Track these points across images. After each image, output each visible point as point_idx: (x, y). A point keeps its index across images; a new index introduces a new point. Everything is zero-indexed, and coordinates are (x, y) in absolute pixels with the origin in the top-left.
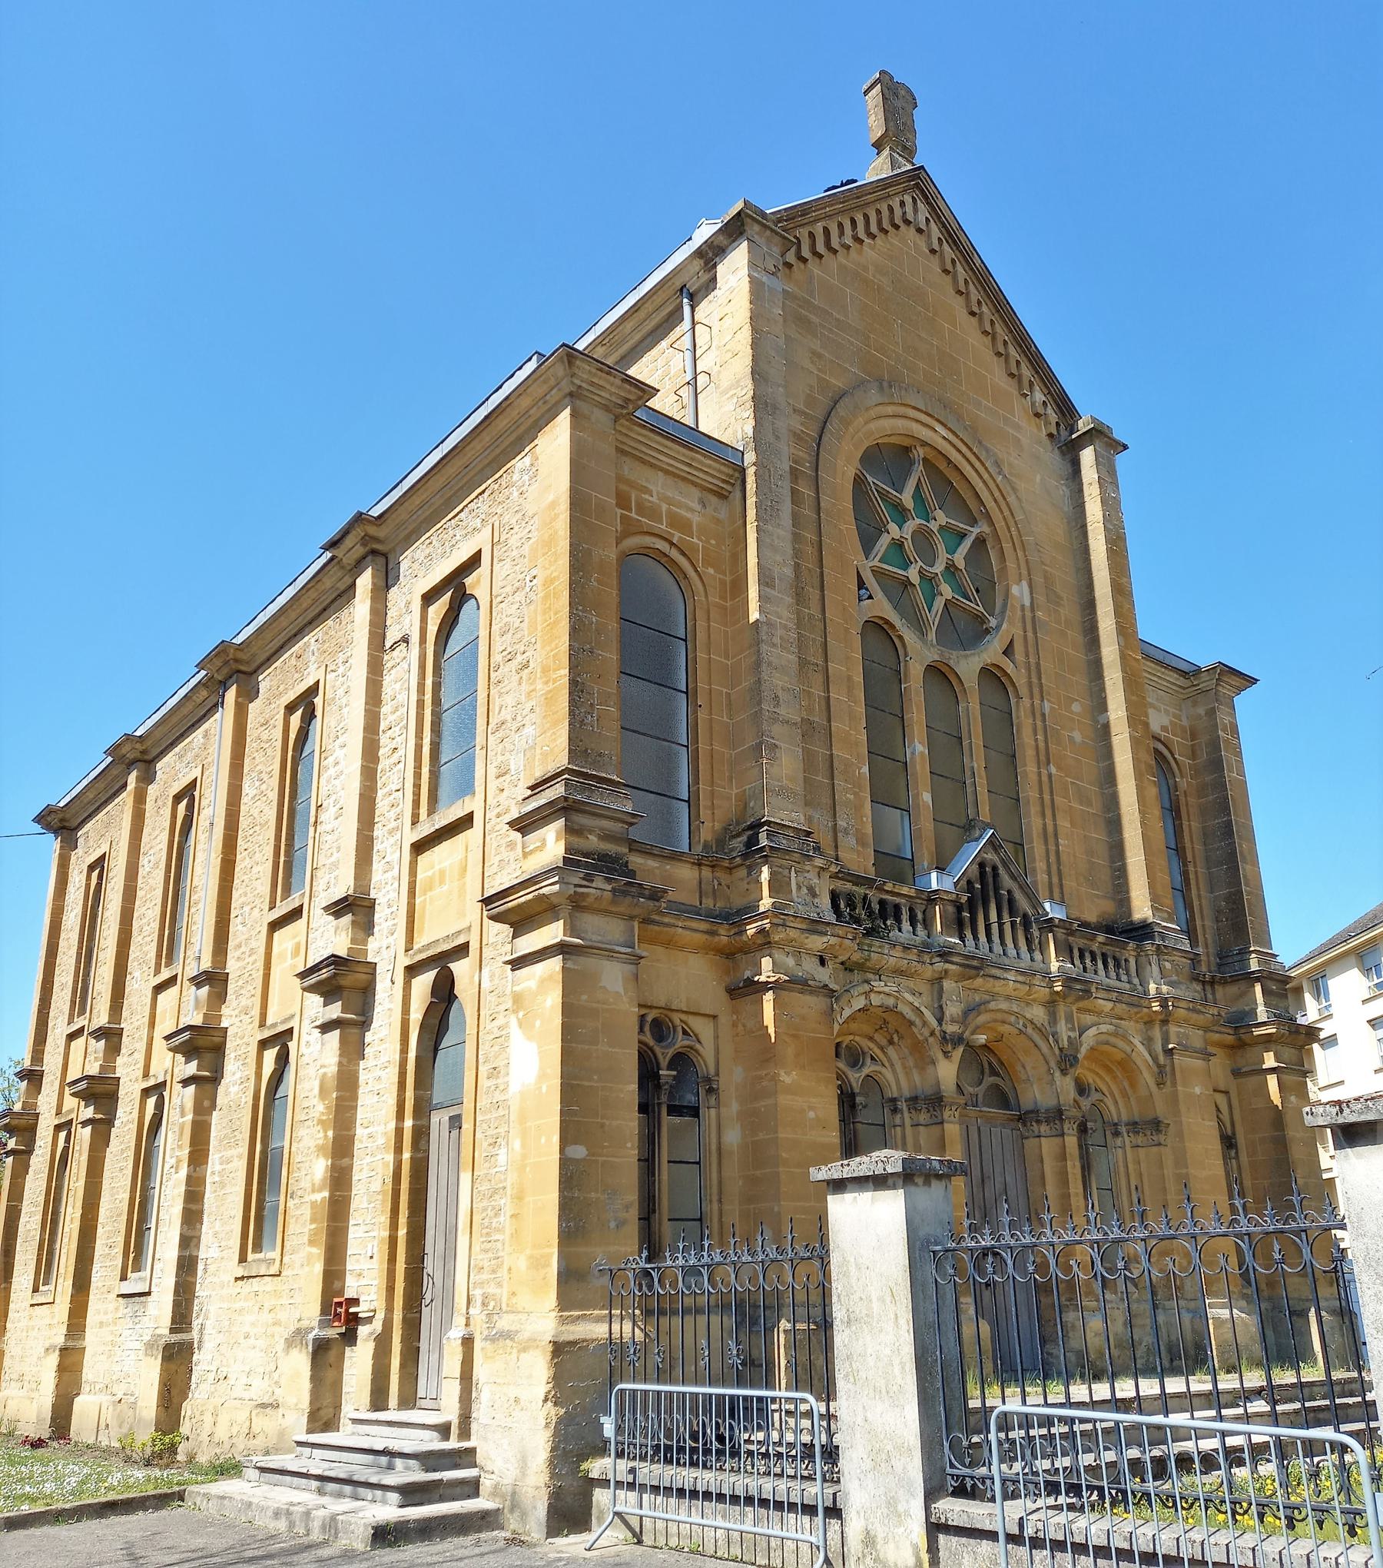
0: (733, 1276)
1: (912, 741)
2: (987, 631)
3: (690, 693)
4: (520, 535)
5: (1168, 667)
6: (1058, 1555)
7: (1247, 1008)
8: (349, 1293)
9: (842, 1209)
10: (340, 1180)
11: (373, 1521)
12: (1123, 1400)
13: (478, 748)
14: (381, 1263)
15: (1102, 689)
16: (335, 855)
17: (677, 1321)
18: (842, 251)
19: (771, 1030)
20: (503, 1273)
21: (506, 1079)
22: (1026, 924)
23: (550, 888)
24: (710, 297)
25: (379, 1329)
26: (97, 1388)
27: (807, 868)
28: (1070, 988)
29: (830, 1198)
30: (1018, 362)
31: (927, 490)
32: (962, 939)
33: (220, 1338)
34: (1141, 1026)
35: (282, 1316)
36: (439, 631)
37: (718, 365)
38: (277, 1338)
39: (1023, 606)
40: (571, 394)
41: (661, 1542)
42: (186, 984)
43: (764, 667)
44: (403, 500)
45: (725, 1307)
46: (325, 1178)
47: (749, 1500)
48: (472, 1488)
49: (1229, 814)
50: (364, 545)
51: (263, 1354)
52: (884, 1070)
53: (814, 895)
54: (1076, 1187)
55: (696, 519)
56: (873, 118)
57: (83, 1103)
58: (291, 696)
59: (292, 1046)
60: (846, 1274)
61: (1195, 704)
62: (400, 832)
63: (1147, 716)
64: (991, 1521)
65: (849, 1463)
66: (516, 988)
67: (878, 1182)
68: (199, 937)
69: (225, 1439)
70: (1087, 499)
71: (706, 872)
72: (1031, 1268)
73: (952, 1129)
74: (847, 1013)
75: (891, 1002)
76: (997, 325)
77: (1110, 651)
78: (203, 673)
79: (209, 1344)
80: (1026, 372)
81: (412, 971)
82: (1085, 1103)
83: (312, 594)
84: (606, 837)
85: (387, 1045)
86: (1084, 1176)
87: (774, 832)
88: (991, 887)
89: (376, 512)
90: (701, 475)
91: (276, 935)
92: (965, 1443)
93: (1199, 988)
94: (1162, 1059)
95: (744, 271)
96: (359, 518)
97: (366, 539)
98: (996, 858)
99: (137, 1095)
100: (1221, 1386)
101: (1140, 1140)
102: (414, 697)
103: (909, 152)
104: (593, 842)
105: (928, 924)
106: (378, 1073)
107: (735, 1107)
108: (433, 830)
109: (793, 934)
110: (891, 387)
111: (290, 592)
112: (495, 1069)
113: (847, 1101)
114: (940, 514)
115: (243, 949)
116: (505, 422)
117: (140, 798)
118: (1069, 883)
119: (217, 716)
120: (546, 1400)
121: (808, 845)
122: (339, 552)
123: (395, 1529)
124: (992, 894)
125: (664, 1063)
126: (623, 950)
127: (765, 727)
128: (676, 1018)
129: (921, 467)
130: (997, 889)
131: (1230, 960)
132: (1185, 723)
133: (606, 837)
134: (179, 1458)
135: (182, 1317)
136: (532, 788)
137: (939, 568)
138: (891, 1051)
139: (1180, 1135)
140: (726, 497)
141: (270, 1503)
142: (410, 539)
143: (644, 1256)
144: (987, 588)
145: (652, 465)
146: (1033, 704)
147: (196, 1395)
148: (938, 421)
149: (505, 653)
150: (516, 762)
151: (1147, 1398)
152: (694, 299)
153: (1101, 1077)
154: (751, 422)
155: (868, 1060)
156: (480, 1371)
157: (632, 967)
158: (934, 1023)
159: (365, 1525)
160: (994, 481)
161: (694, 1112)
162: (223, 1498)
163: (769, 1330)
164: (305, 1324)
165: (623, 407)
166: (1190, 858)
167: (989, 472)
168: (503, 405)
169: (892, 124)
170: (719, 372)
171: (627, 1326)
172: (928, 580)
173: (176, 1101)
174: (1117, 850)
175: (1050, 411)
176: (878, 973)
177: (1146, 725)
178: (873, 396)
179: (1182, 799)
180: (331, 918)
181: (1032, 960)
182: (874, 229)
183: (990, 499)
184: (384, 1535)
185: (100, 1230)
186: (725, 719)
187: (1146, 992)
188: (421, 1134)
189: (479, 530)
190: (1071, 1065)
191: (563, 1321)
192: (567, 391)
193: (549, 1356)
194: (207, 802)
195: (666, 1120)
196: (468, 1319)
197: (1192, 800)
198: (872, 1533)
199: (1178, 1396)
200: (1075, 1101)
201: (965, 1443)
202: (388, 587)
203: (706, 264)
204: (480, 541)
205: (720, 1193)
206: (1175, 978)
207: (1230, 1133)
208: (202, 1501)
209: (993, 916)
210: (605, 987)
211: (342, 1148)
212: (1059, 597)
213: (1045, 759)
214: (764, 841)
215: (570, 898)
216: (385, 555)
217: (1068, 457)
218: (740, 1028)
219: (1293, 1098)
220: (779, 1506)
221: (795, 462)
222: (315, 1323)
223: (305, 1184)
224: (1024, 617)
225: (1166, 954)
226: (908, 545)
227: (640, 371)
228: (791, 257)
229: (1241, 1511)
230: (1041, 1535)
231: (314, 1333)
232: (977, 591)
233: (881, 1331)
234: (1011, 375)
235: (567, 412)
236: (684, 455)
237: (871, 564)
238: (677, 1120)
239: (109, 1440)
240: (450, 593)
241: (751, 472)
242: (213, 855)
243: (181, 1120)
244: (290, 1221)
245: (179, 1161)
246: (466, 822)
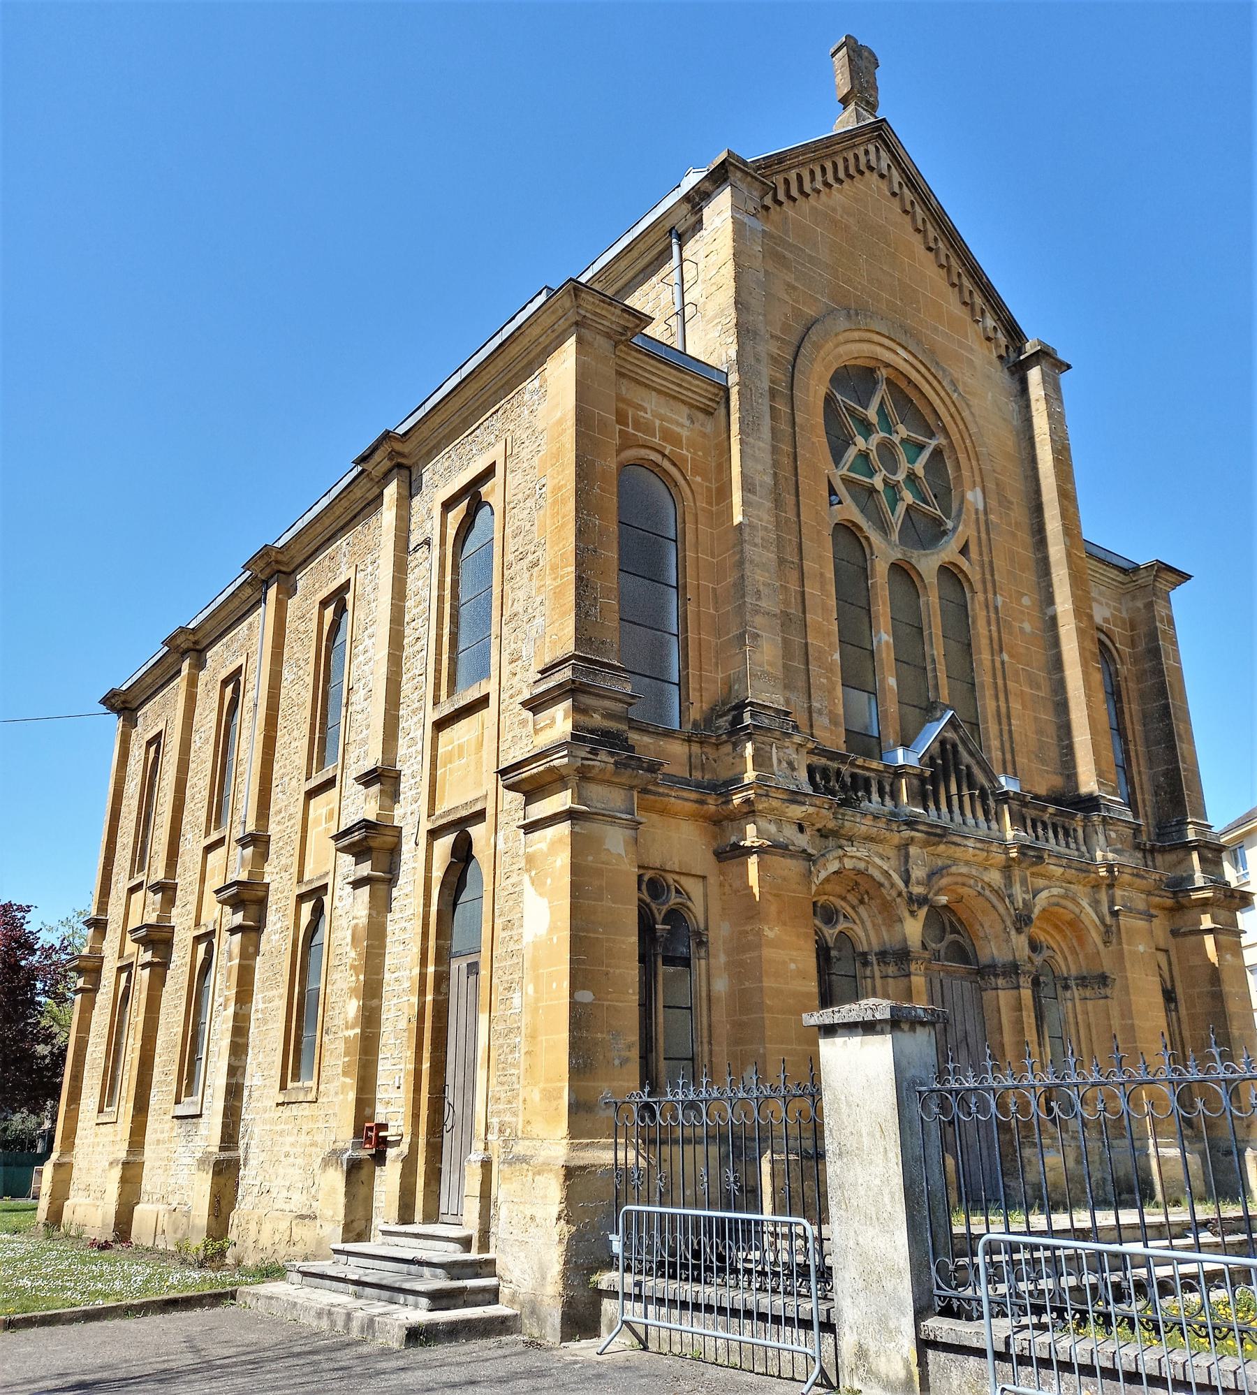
0: (730, 1111)
1: (878, 632)
2: (945, 533)
3: (680, 588)
4: (530, 449)
5: (1109, 564)
6: (1043, 1371)
7: (1184, 875)
8: (379, 1119)
9: (832, 1052)
10: (370, 1019)
11: (408, 1323)
12: (1082, 1230)
13: (493, 637)
14: (407, 1092)
15: (1050, 585)
16: (365, 732)
17: (677, 1150)
18: (813, 195)
19: (756, 890)
21: (520, 931)
22: (984, 796)
23: (559, 761)
24: (697, 237)
25: (406, 1151)
26: (155, 1198)
27: (786, 744)
28: (1024, 854)
29: (821, 1041)
30: (971, 292)
31: (889, 403)
32: (926, 810)
33: (263, 1156)
34: (1088, 889)
35: (319, 1138)
36: (457, 534)
37: (704, 297)
38: (314, 1157)
39: (977, 511)
40: (577, 323)
41: (665, 1349)
42: (233, 844)
44: (425, 419)
45: (723, 1139)
46: (356, 1018)
47: (748, 1314)
48: (492, 1295)
49: (1167, 698)
50: (391, 459)
51: (301, 1171)
52: (855, 927)
53: (793, 769)
54: (1031, 1035)
55: (685, 433)
56: (840, 77)
57: (142, 948)
59: (327, 900)
60: (838, 1111)
61: (1134, 598)
62: (422, 712)
63: (1091, 608)
64: (978, 1339)
65: (844, 1281)
67: (868, 1027)
68: (244, 804)
69: (269, 1246)
70: (1034, 413)
71: (696, 748)
72: (1013, 1109)
73: (918, 981)
74: (823, 875)
75: (862, 865)
76: (952, 259)
77: (1056, 550)
78: (248, 573)
79: (253, 1162)
80: (978, 300)
81: (434, 834)
82: (1038, 960)
83: (345, 503)
84: (609, 715)
85: (412, 900)
86: (1037, 1025)
87: (756, 712)
88: (951, 763)
89: (401, 430)
90: (690, 394)
91: (312, 802)
92: (951, 1267)
93: (1140, 855)
94: (1108, 919)
95: (728, 213)
96: (387, 436)
97: (393, 454)
98: (955, 736)
99: (190, 942)
100: (1171, 1219)
101: (1088, 993)
102: (435, 593)
103: (872, 107)
104: (597, 720)
105: (895, 795)
106: (404, 924)
107: (723, 959)
108: (452, 709)
109: (775, 803)
110: (857, 314)
111: (325, 502)
112: (509, 921)
113: (823, 954)
114: (901, 428)
115: (283, 815)
116: (517, 349)
117: (192, 683)
118: (1021, 760)
119: (260, 610)
120: (559, 1218)
121: (788, 724)
122: (369, 466)
123: (426, 1330)
125: (659, 918)
126: (624, 816)
127: (748, 617)
128: (670, 878)
129: (884, 387)
131: (1169, 830)
132: (1124, 615)
133: (609, 715)
134: (227, 1261)
135: (230, 1137)
136: (542, 672)
137: (901, 476)
138: (861, 909)
139: (1126, 989)
140: (712, 414)
141: (313, 1304)
142: (431, 454)
143: (646, 1090)
144: (944, 494)
145: (647, 386)
146: (986, 599)
147: (242, 1207)
148: (899, 344)
149: (517, 553)
150: (526, 650)
151: (1103, 1228)
152: (682, 239)
153: (1048, 933)
154: (735, 347)
155: (842, 918)
156: (500, 1191)
157: (632, 832)
158: (901, 884)
159: (400, 1327)
160: (951, 398)
161: (686, 962)
162: (271, 1298)
163: (755, 1162)
164: (340, 1145)
165: (622, 334)
167: (945, 390)
168: (516, 334)
169: (856, 82)
170: (705, 303)
171: (632, 1154)
172: (892, 487)
173: (224, 947)
174: (1065, 730)
175: (1000, 335)
176: (850, 840)
177: (1091, 617)
178: (842, 323)
179: (1123, 684)
180: (362, 787)
181: (989, 828)
182: (841, 175)
183: (947, 414)
184: (415, 1335)
185: (157, 1059)
186: (711, 611)
187: (1093, 859)
188: (442, 979)
189: (493, 445)
190: (1026, 925)
191: (574, 1148)
192: (573, 320)
193: (561, 1179)
194: (251, 685)
195: (661, 969)
196: (486, 1144)
197: (1131, 685)
198: (865, 1347)
199: (1132, 1227)
200: (1029, 958)
201: (951, 1267)
202: (411, 497)
203: (693, 208)
204: (495, 454)
205: (710, 1036)
206: (1119, 846)
207: (1169, 987)
208: (252, 1301)
209: (954, 789)
210: (608, 850)
211: (372, 991)
212: (1009, 502)
213: (998, 647)
214: (747, 720)
215: (578, 770)
216: (409, 468)
217: (1017, 376)
218: (727, 887)
219: (1228, 957)
220: (776, 1320)
222: (349, 1145)
223: (339, 1021)
224: (977, 519)
225: (1111, 824)
226: (874, 456)
227: (635, 301)
228: (768, 201)
229: (1220, 1336)
230: (1026, 1353)
231: (348, 1154)
232: (935, 497)
233: (871, 1163)
234: (965, 303)
235: (573, 339)
236: (674, 376)
237: (840, 473)
238: (671, 969)
239: (167, 1244)
240: (467, 501)
241: (734, 392)
242: (257, 732)
243: (229, 964)
244: (325, 1053)
245: (227, 1000)
246: (483, 702)
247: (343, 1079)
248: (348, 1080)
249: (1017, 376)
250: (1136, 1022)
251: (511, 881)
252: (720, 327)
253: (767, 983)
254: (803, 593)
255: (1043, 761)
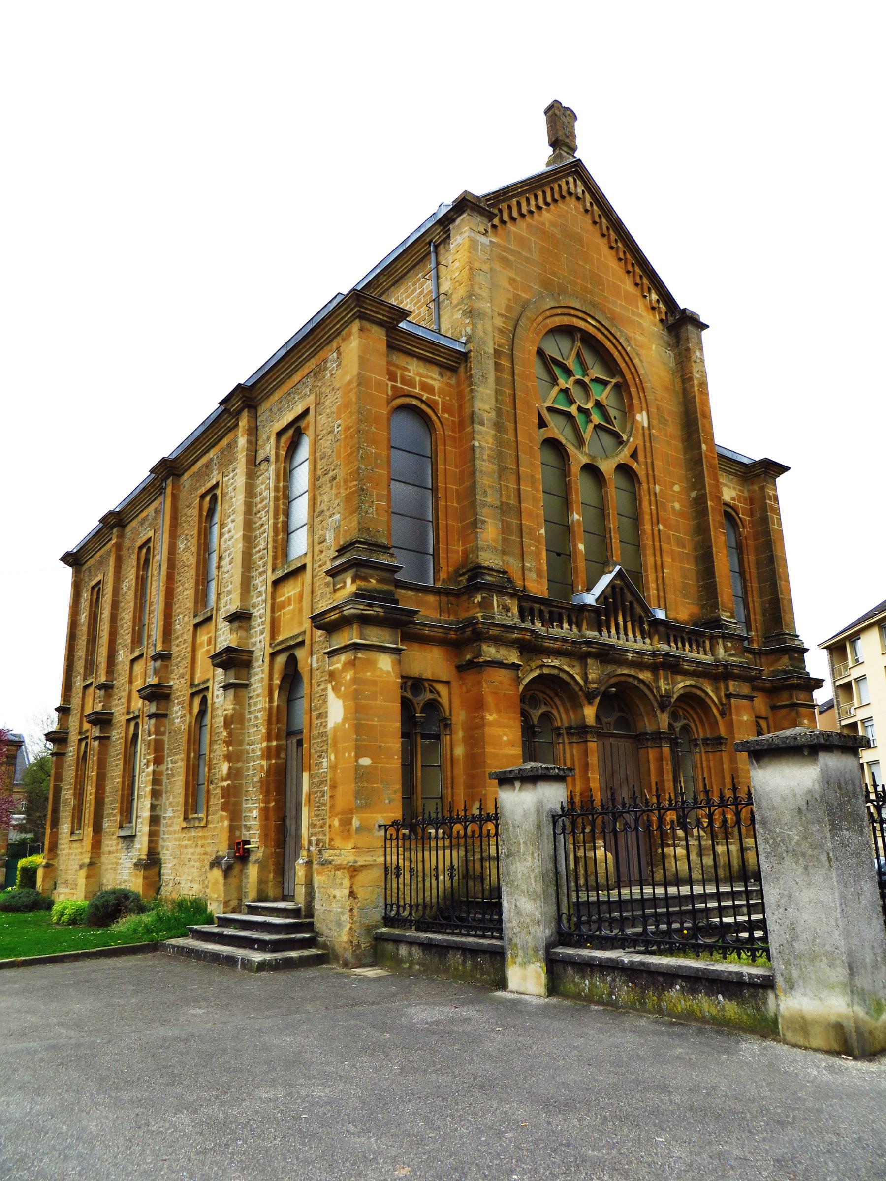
1: (572, 513)
16: (230, 586)
20: (326, 828)
23: (348, 611)
39: (643, 427)
42: (149, 659)
43: (478, 474)
58: (203, 490)
66: (331, 668)
115: (180, 640)
118: (670, 596)
124: (619, 605)
125: (418, 709)
130: (623, 602)
146: (649, 488)
161: (437, 737)
166: (748, 578)
175: (661, 305)
182: (549, 199)
197: (751, 542)
203: (444, 228)
206: (733, 652)
209: (621, 619)
212: (666, 420)
217: (673, 333)
221: (499, 346)
224: (644, 434)
245: (148, 761)
247: (221, 813)
248: (224, 814)
249: (673, 333)
250: (740, 766)
251: (322, 687)
252: (461, 312)
253: (489, 750)
254: (519, 490)
255: (685, 596)
